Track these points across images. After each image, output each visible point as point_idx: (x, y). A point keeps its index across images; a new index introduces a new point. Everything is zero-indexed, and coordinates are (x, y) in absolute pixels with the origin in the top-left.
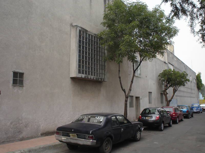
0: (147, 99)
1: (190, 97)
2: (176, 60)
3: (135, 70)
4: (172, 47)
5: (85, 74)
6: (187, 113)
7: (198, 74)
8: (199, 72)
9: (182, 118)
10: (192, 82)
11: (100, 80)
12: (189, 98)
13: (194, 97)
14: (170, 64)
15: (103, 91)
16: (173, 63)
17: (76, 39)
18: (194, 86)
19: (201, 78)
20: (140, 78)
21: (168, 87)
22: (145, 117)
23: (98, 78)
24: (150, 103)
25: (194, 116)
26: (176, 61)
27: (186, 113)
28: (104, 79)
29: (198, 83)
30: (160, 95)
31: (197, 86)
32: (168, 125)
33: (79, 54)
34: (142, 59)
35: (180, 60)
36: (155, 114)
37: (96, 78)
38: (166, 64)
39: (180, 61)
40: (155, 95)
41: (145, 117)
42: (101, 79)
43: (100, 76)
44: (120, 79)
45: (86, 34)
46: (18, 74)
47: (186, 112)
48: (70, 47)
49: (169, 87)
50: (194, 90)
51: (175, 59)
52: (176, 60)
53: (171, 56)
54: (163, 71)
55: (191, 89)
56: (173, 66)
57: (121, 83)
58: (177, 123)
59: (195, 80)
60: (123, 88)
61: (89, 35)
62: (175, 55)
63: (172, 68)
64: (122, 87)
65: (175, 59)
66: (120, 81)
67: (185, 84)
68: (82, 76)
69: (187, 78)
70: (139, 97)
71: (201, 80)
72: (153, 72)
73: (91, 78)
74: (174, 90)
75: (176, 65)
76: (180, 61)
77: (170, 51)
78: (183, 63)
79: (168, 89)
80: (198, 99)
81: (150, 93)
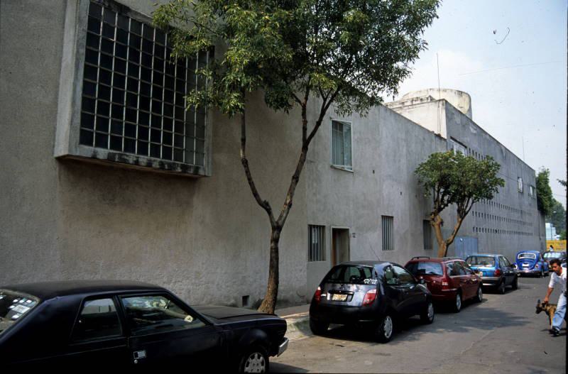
0: (375, 237)
1: (519, 233)
2: (475, 132)
3: (307, 137)
4: (465, 100)
5: (111, 148)
6: (496, 278)
7: (540, 174)
9: (478, 293)
10: (522, 193)
11: (179, 170)
13: (532, 234)
14: (456, 141)
15: (201, 207)
16: (466, 140)
17: (75, 31)
18: (530, 205)
20: (351, 175)
21: (446, 202)
22: (330, 292)
23: (172, 167)
24: (387, 245)
25: (519, 284)
26: (475, 134)
27: (493, 278)
28: (197, 169)
30: (421, 227)
32: (510, 286)
33: (85, 83)
34: (327, 103)
35: (486, 133)
37: (161, 162)
38: (443, 141)
39: (488, 137)
40: (405, 223)
41: (333, 292)
42: (185, 168)
43: (178, 158)
44: (245, 166)
45: (124, 18)
47: (494, 276)
48: (62, 58)
49: (449, 202)
50: (530, 214)
51: (472, 130)
52: (475, 132)
53: (458, 119)
54: (428, 159)
55: (522, 212)
56: (466, 147)
57: (250, 179)
58: (456, 311)
59: (533, 188)
60: (263, 199)
61: (137, 24)
62: (474, 120)
63: (464, 152)
64: (256, 195)
65: (471, 128)
66: (247, 172)
67: (494, 194)
68: (95, 152)
69: (497, 176)
70: (348, 230)
71: (549, 188)
72: (400, 161)
73: (137, 163)
74: (459, 211)
75: (474, 145)
76: (488, 137)
77: (459, 109)
78: (498, 142)
79: (444, 208)
81: (387, 219)
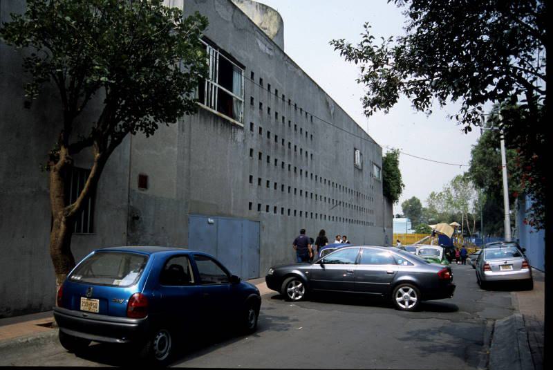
8: (361, 99)
10: (361, 170)
12: (346, 224)
19: (400, 167)
29: (387, 180)
31: (384, 191)
35: (298, 67)
36: (395, 306)
46: (423, 302)
50: (371, 199)
62: (285, 52)
71: (398, 171)
76: (300, 74)
80: (384, 231)
